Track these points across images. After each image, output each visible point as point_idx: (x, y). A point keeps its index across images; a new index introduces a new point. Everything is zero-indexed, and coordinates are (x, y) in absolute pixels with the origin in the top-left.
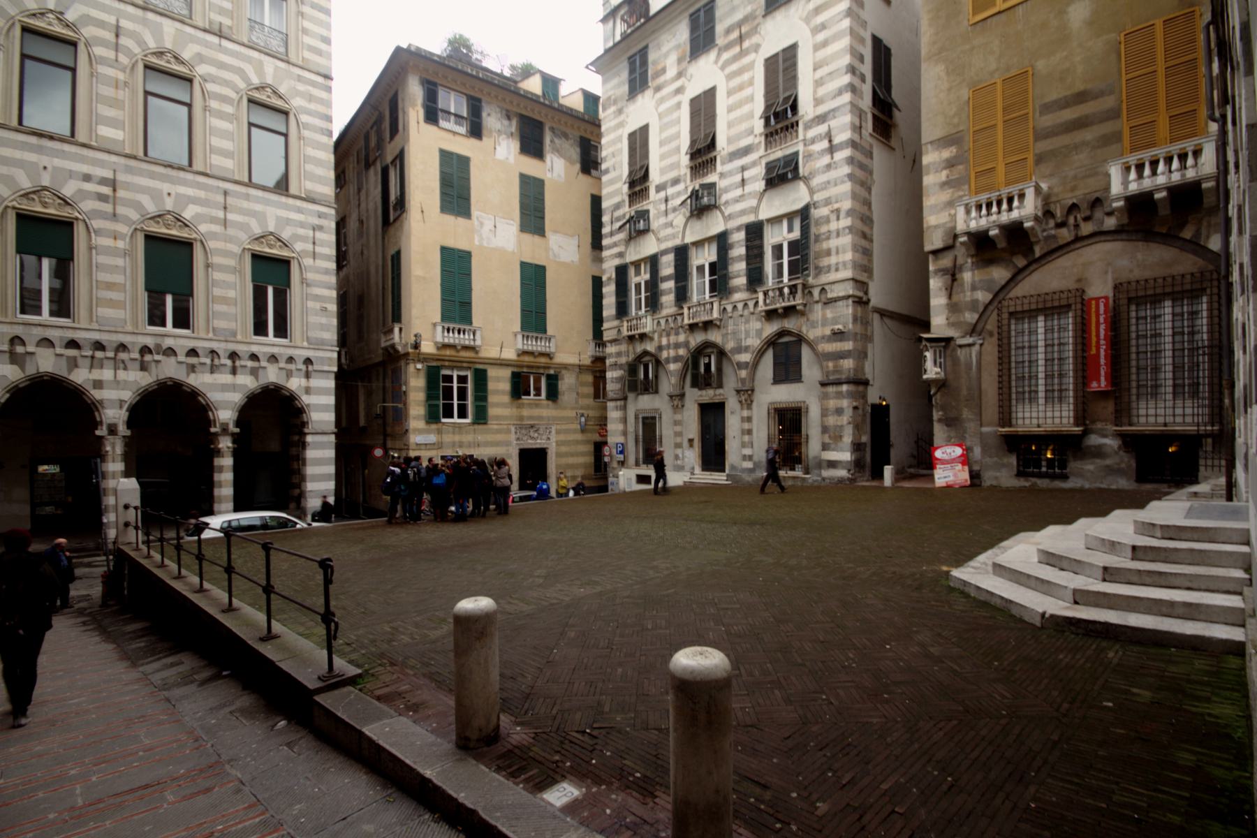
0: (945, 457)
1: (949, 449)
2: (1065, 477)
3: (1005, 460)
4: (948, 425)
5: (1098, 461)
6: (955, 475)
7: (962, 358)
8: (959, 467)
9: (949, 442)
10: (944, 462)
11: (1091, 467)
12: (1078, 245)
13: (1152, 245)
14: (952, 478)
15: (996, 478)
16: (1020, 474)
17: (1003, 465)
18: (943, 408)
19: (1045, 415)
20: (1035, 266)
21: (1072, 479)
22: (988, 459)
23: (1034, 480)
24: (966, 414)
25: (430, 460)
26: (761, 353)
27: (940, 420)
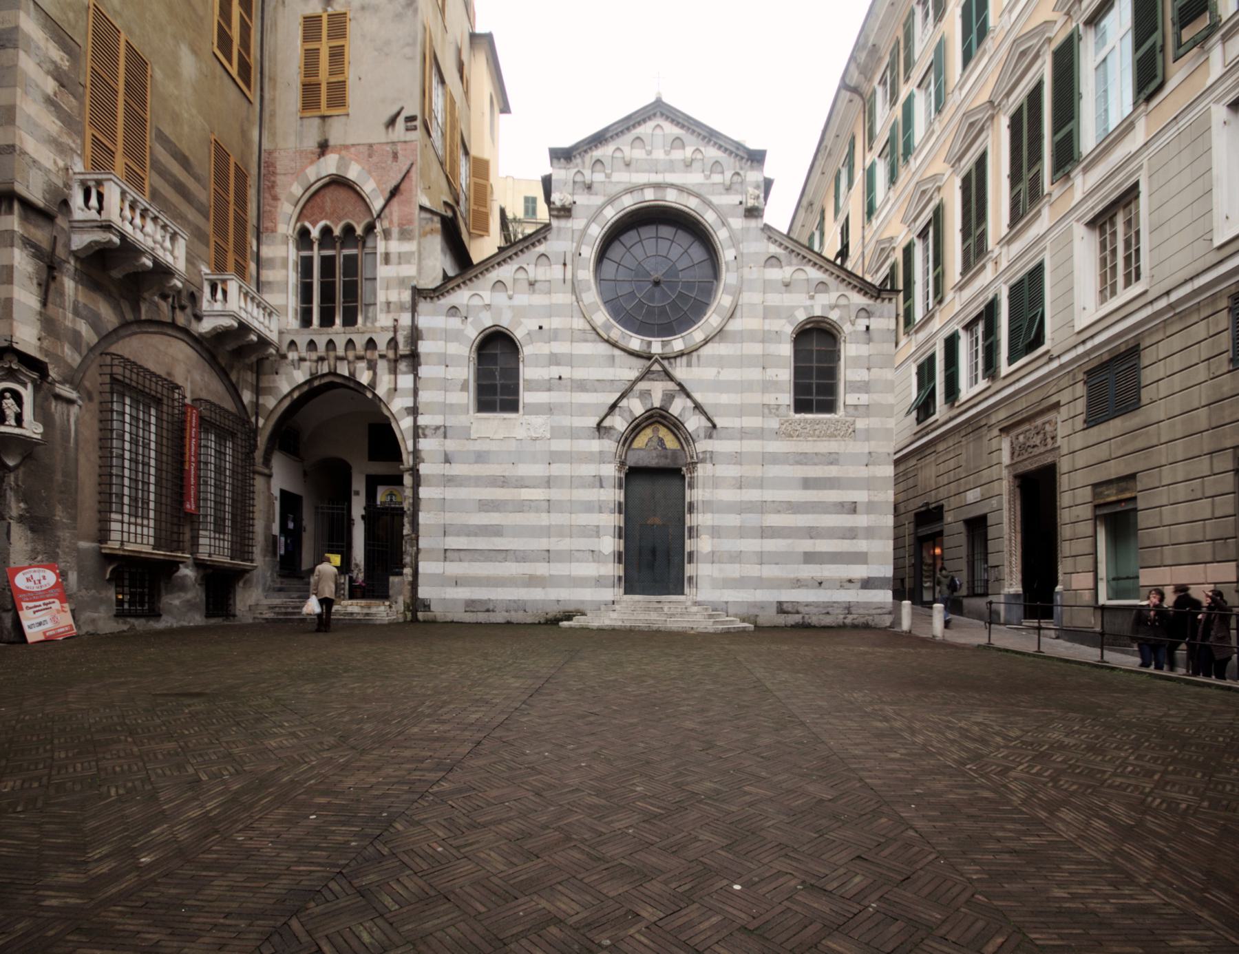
0: (32, 587)
1: (37, 574)
2: (155, 614)
3: (104, 594)
4: (33, 530)
5: (182, 594)
6: (54, 619)
7: (57, 417)
8: (57, 605)
9: (34, 560)
10: (33, 596)
11: (177, 602)
12: (170, 332)
13: (38, 323)
14: (49, 625)
15: (93, 621)
16: (120, 615)
17: (102, 601)
18: (24, 497)
19: (134, 535)
20: (135, 328)
21: (164, 617)
22: (84, 592)
23: (132, 620)
24: (60, 515)
25: (1182, 590)
26: (233, 317)
27: (21, 519)
